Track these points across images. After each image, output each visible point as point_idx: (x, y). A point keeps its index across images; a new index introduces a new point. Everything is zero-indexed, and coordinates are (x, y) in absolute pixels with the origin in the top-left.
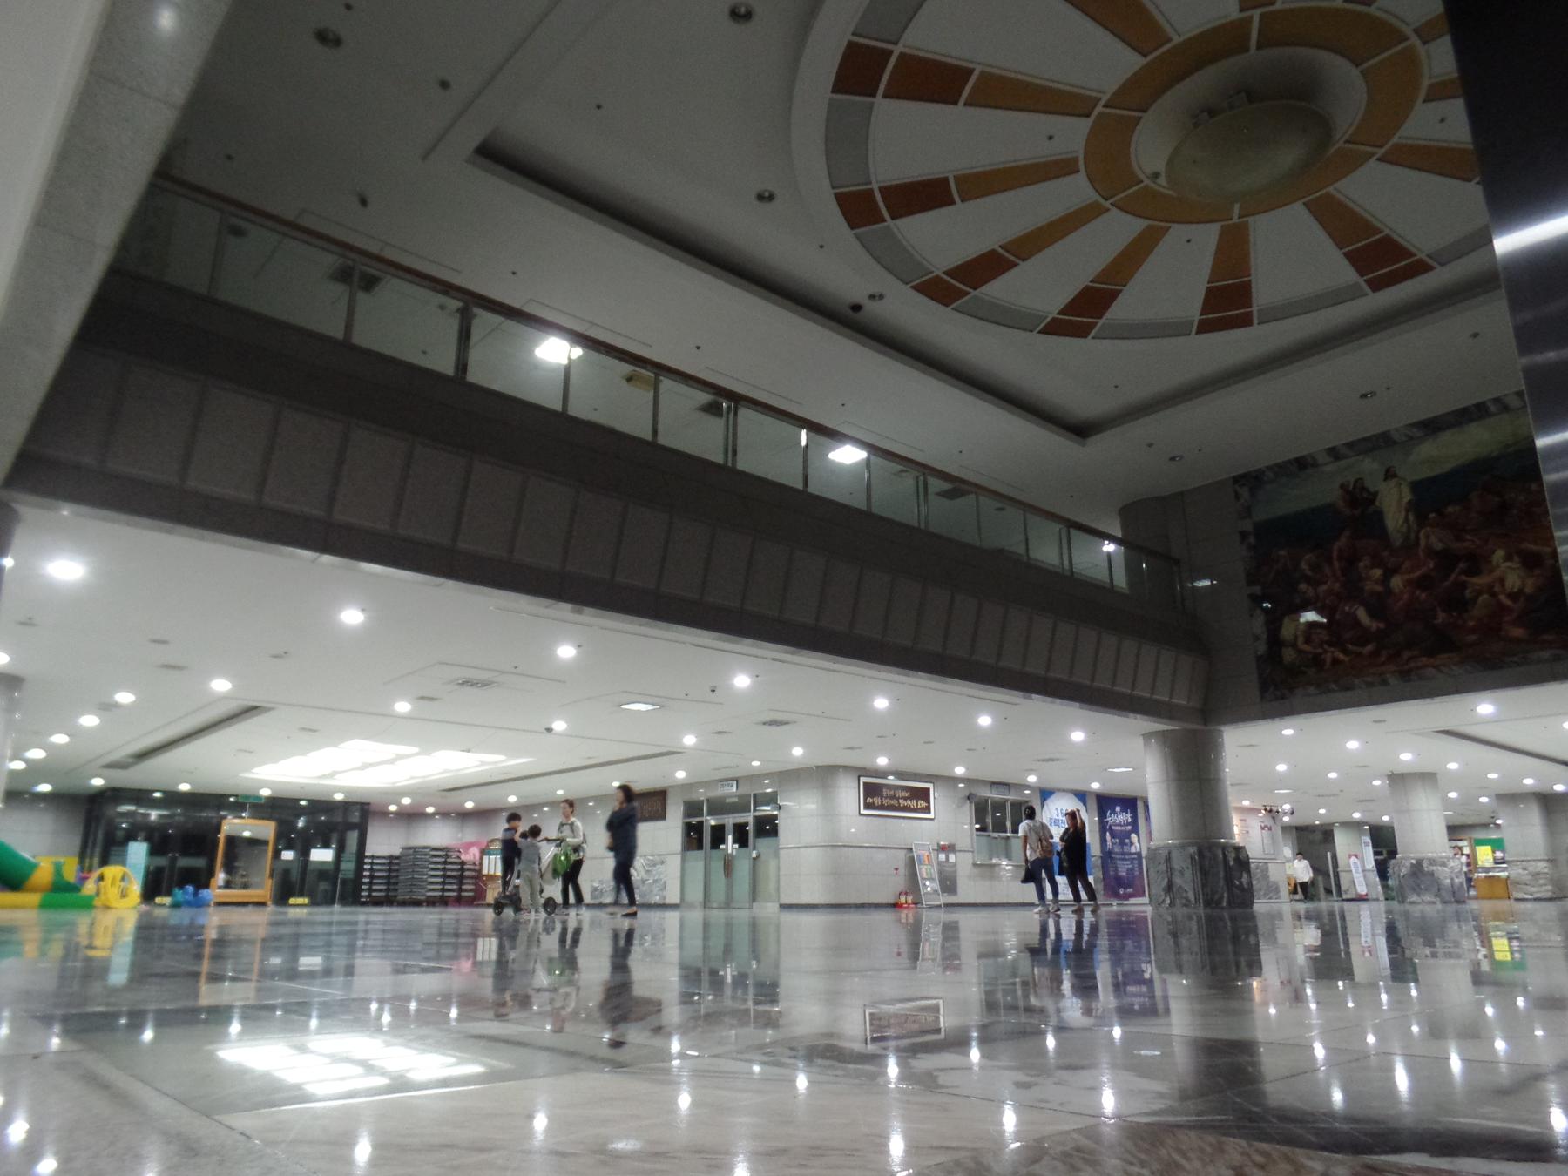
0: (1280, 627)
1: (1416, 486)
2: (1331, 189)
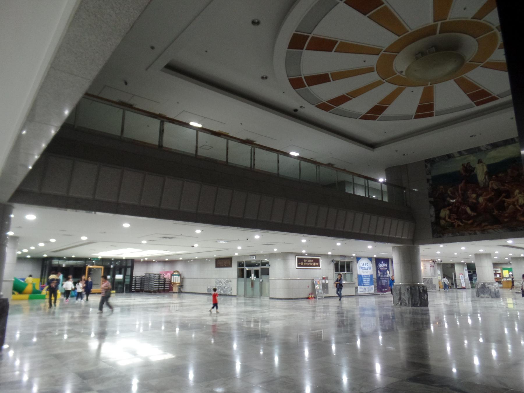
0: (439, 213)
1: (489, 166)
2: (463, 76)
